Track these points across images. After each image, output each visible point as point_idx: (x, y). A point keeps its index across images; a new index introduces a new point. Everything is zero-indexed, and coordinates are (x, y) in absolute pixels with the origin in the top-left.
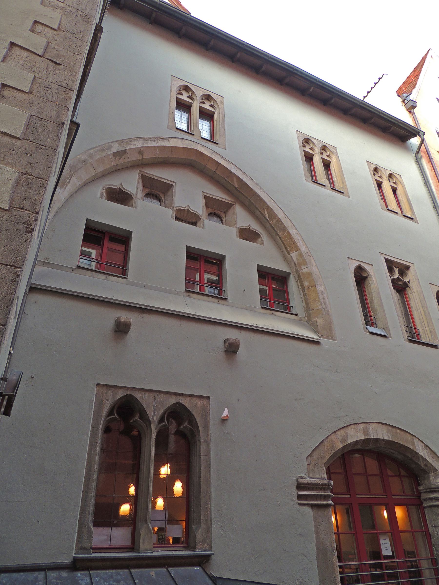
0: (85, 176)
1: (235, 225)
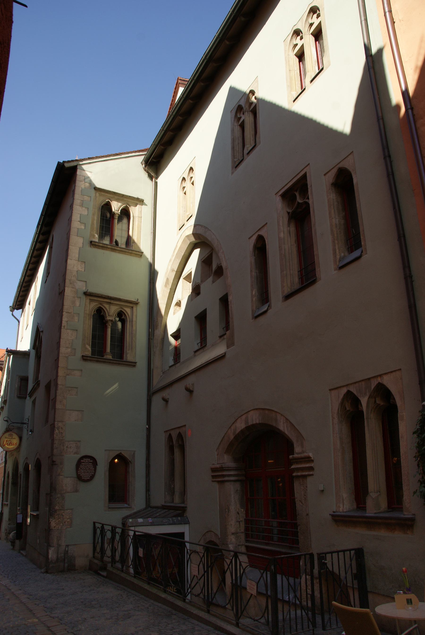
1: (202, 281)
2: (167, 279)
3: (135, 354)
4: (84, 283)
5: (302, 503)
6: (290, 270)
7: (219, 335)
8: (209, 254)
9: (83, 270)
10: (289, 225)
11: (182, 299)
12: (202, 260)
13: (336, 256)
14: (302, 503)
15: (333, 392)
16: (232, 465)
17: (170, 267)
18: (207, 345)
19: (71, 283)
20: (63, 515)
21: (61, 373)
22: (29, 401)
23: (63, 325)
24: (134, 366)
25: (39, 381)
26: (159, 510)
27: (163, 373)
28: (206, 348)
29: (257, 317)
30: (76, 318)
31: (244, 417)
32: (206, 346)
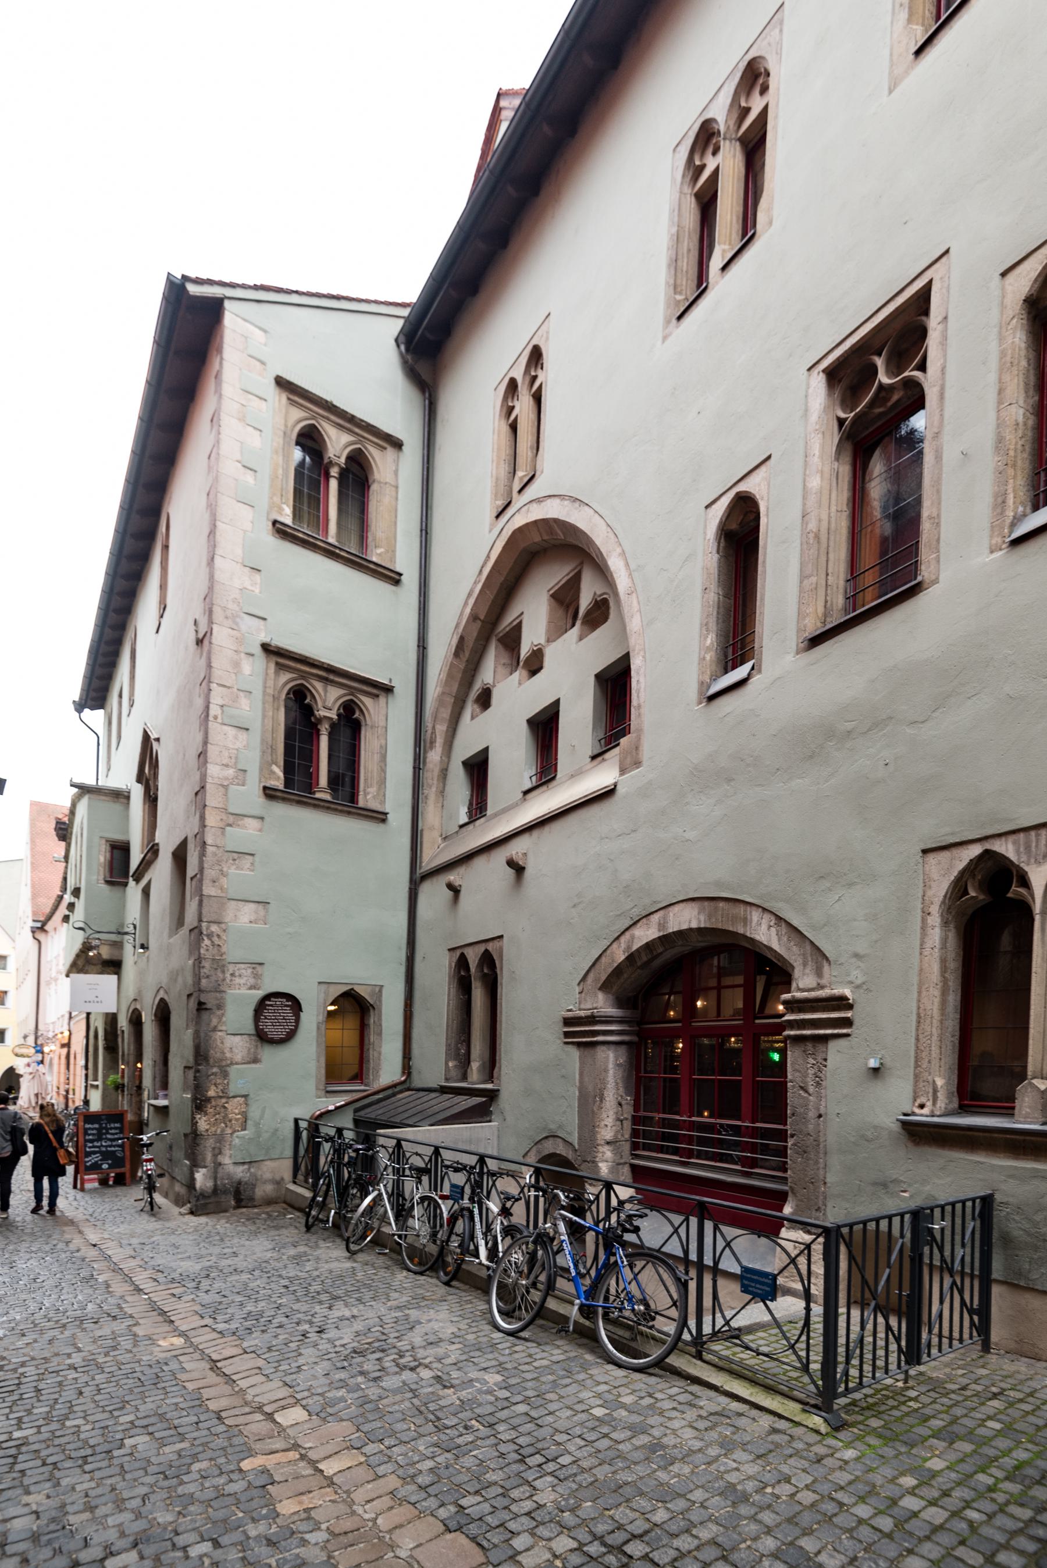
0: (446, 713)
1: (548, 641)
2: (462, 639)
3: (384, 795)
4: (262, 622)
5: (806, 1091)
6: (827, 575)
7: (590, 753)
8: (571, 575)
9: (257, 591)
10: (837, 459)
11: (494, 686)
12: (552, 592)
13: (1002, 513)
14: (806, 1091)
15: (932, 859)
16: (611, 1011)
17: (468, 610)
18: (559, 775)
19: (227, 618)
20: (225, 1107)
21: (212, 819)
22: (134, 890)
23: (212, 713)
24: (384, 821)
25: (157, 844)
26: (433, 1095)
27: (445, 839)
28: (554, 783)
29: (712, 698)
30: (244, 703)
31: (656, 917)
32: (554, 778)
